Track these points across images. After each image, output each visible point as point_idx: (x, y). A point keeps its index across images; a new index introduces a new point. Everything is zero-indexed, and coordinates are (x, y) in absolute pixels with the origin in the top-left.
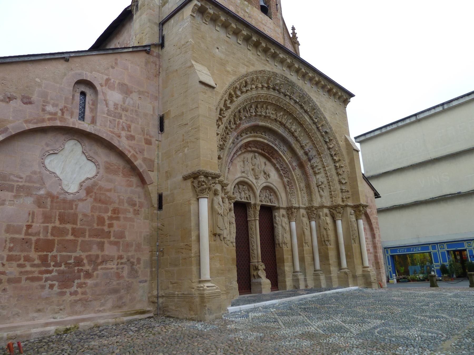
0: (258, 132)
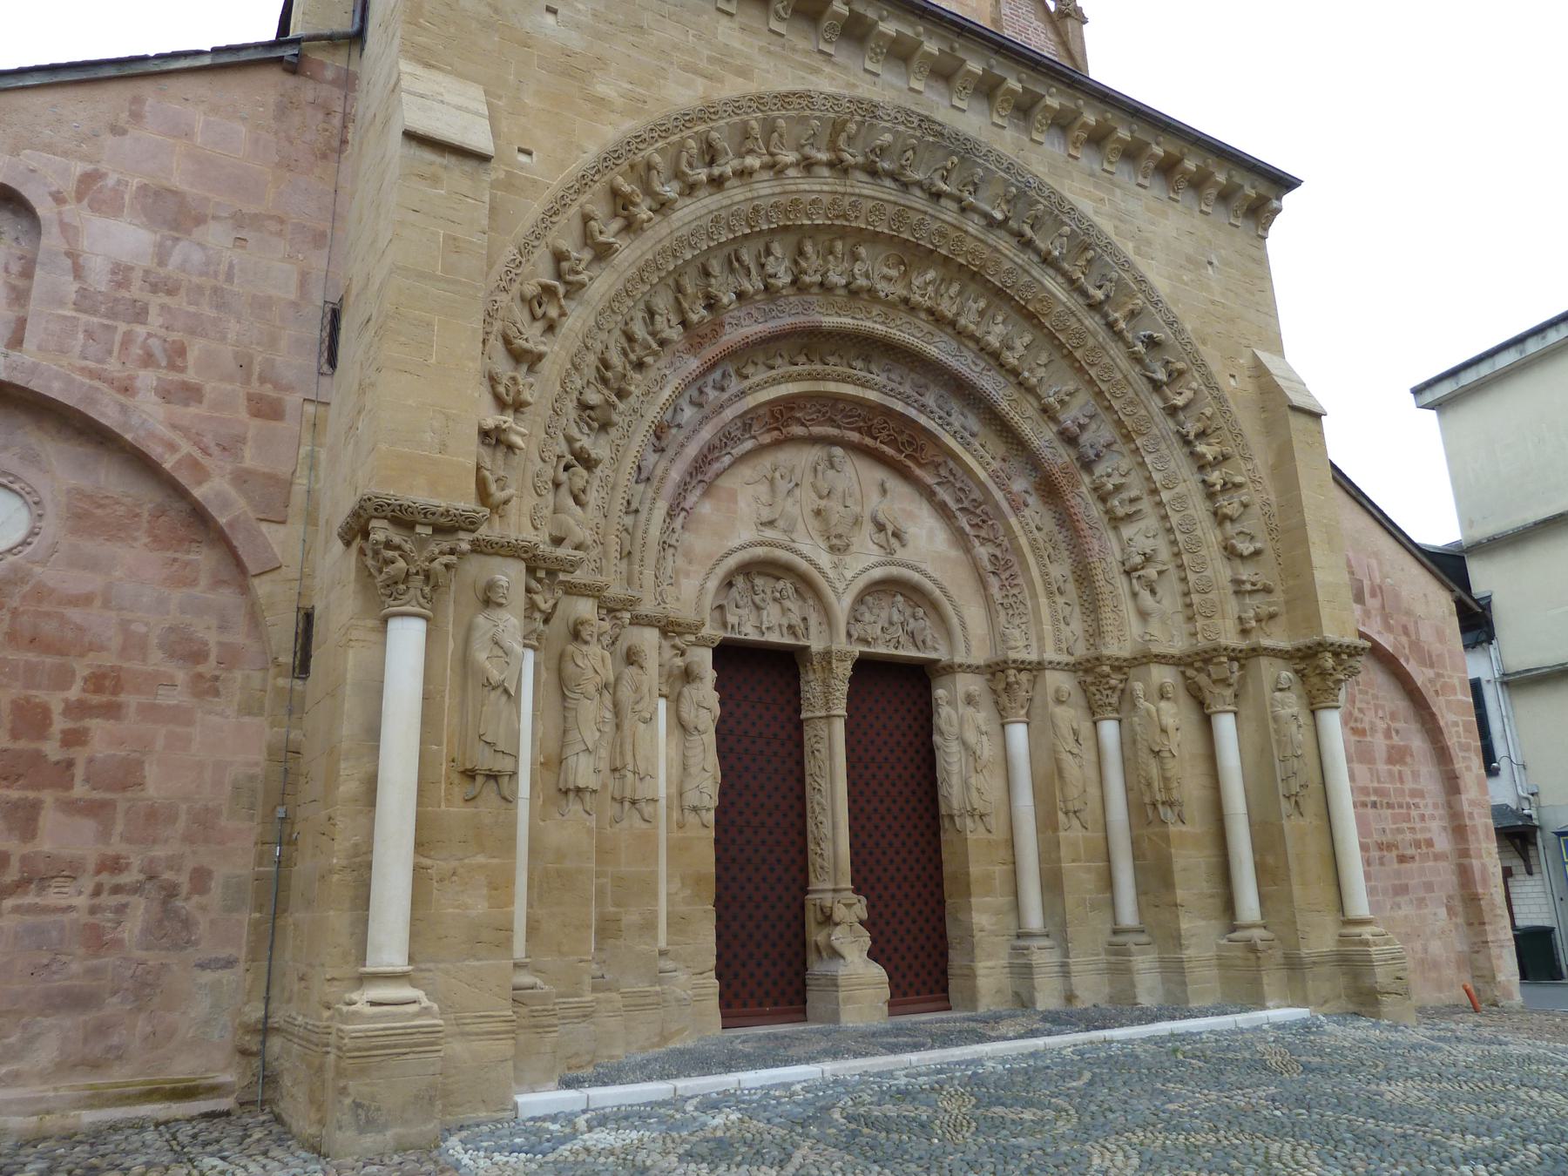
0: (832, 360)
